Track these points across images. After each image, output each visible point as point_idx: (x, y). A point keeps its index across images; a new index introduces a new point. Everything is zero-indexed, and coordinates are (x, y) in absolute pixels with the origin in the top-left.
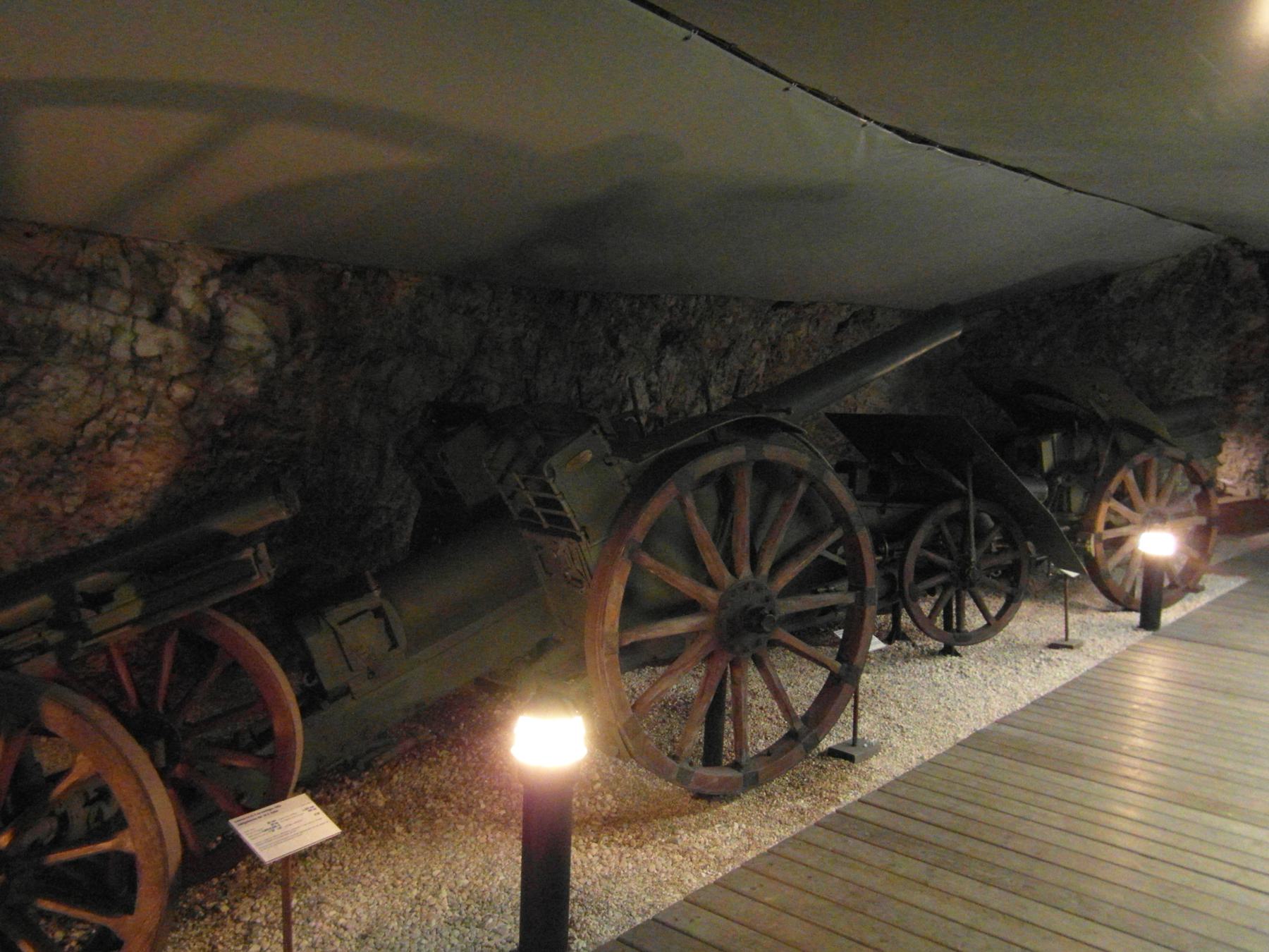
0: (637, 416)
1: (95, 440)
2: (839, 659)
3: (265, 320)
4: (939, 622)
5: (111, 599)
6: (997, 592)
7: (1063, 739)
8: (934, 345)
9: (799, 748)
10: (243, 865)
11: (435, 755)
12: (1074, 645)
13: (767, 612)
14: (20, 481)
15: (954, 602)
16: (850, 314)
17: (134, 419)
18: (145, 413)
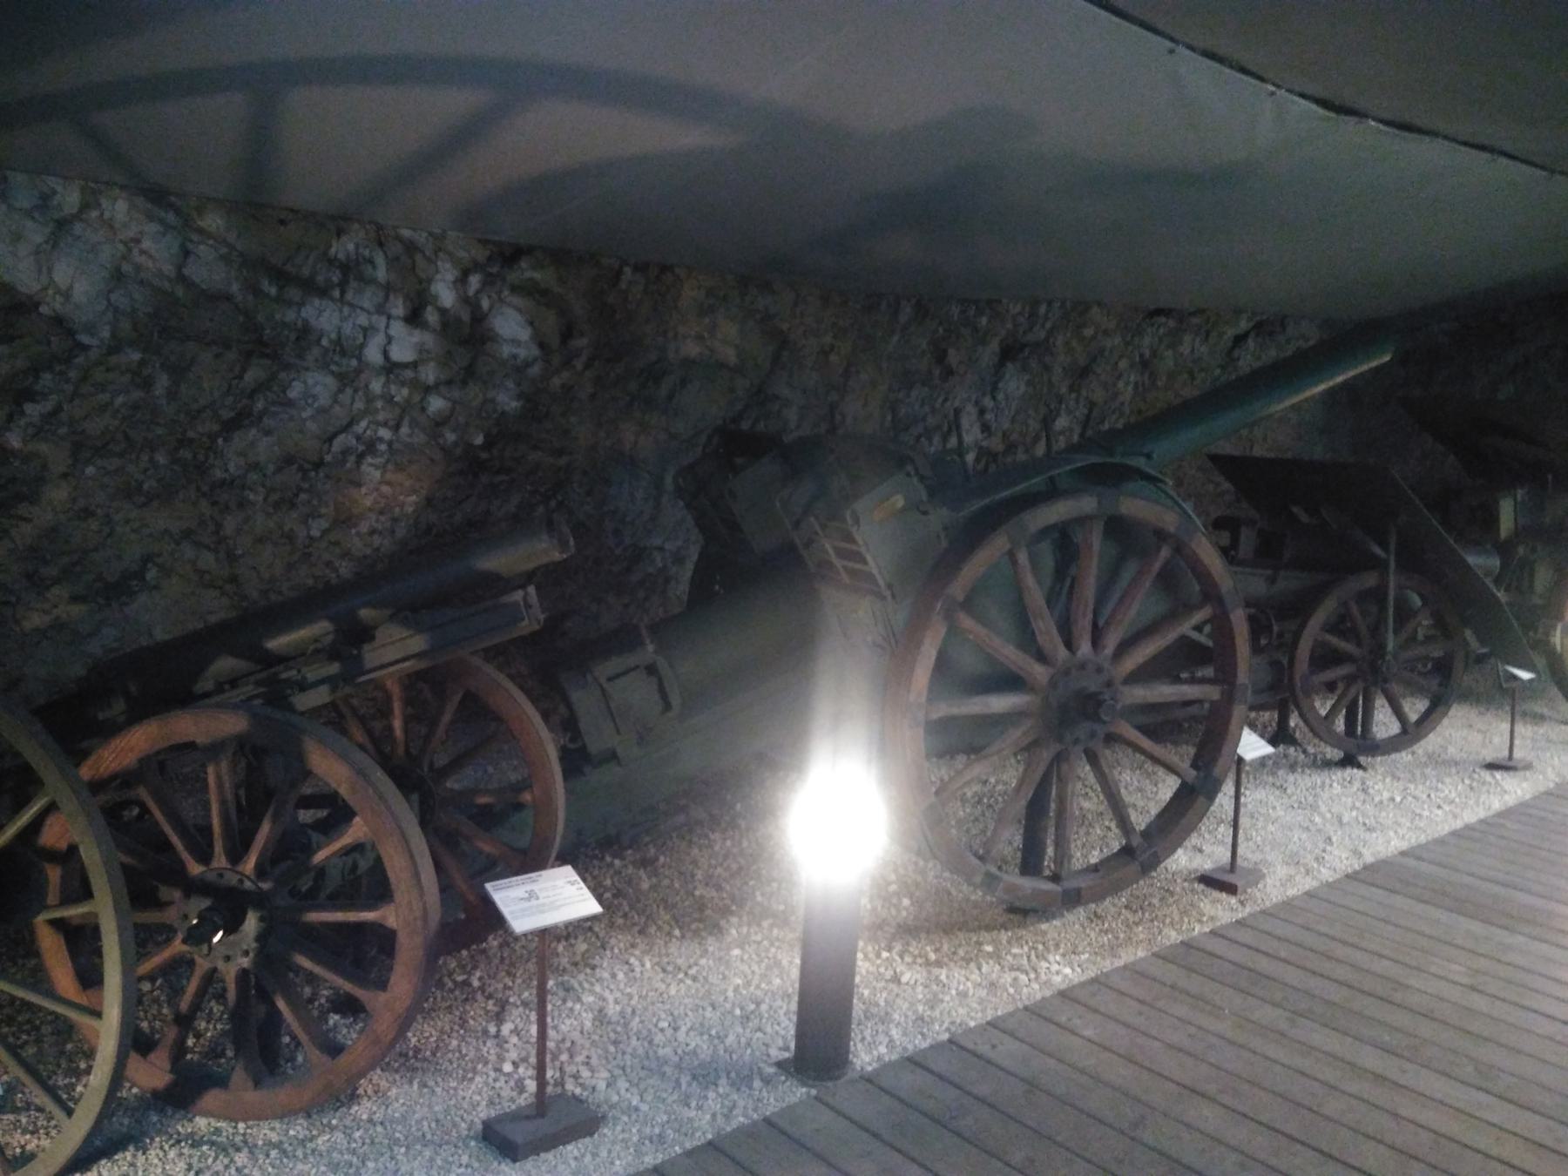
0: (961, 455)
1: (346, 452)
3: (531, 324)
4: (1340, 725)
5: (372, 638)
6: (1419, 691)
7: (1497, 883)
8: (1365, 367)
9: (1134, 867)
10: (495, 939)
11: (707, 836)
12: (1520, 765)
13: (1106, 697)
14: (265, 499)
15: (1361, 698)
16: (1251, 324)
17: (385, 433)
18: (397, 428)
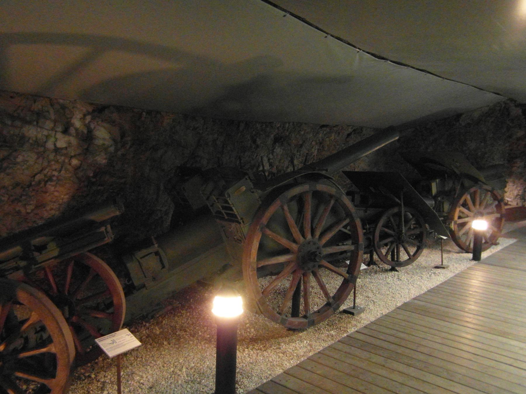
0: (264, 172)
2: (348, 273)
3: (110, 133)
4: (389, 257)
5: (46, 248)
6: (413, 245)
7: (441, 306)
8: (387, 143)
11: (180, 312)
12: (445, 267)
13: (318, 253)
15: (396, 249)
16: (352, 130)
17: (56, 173)
18: (60, 171)
